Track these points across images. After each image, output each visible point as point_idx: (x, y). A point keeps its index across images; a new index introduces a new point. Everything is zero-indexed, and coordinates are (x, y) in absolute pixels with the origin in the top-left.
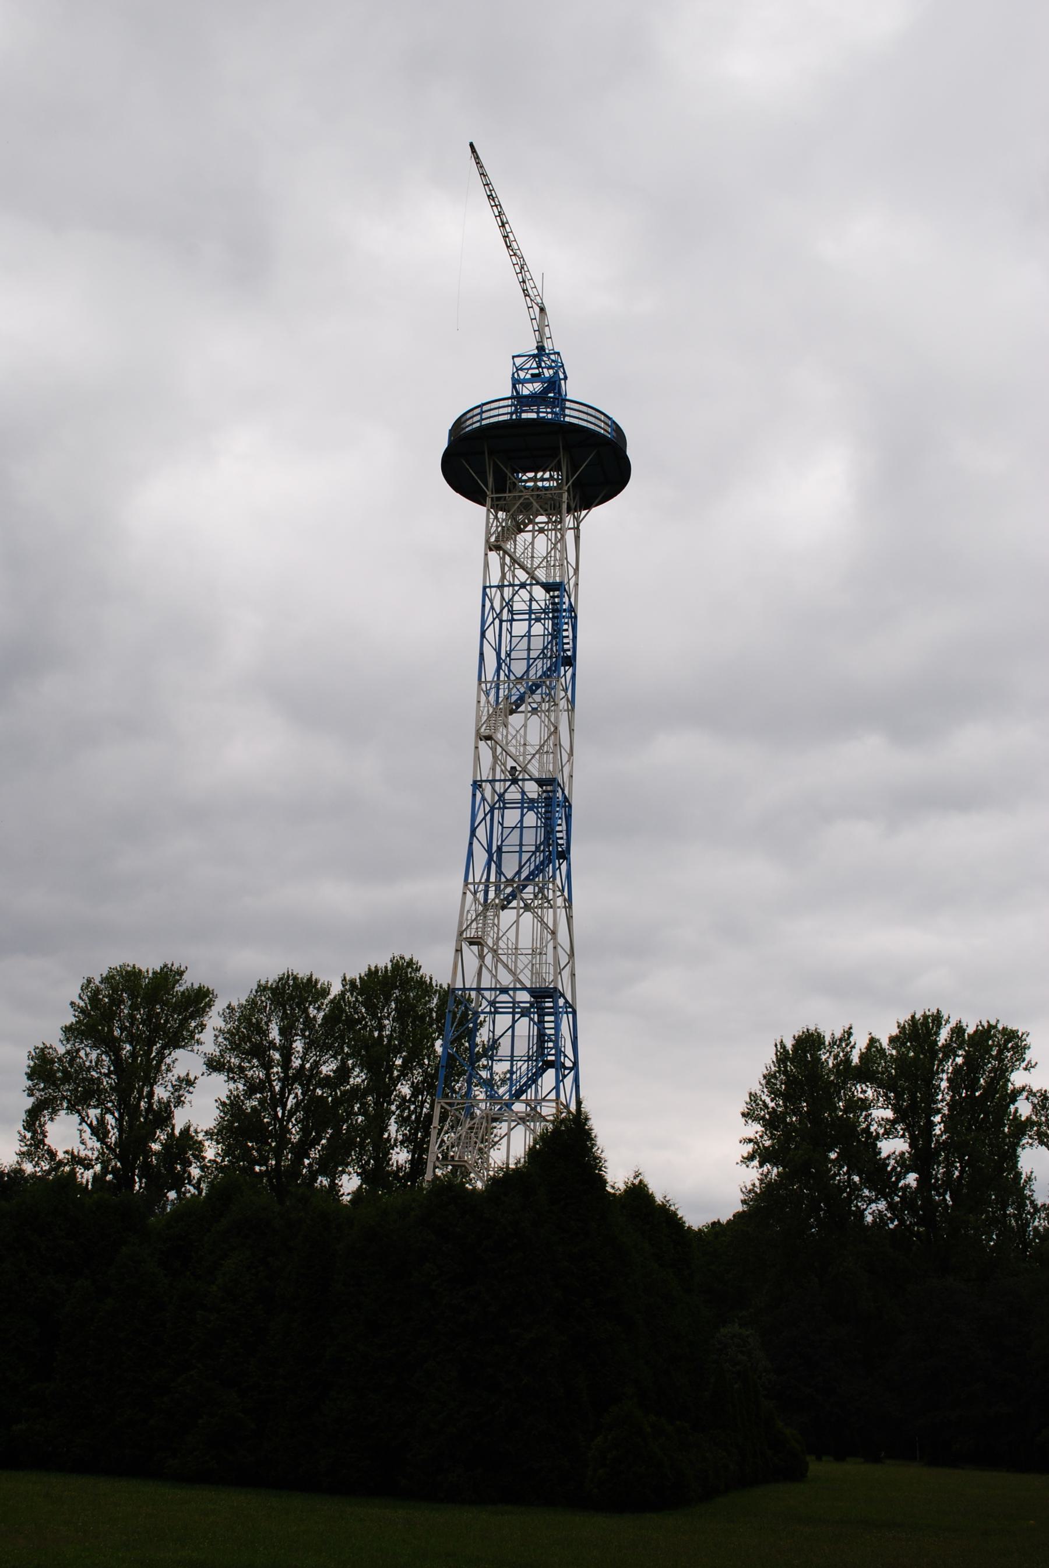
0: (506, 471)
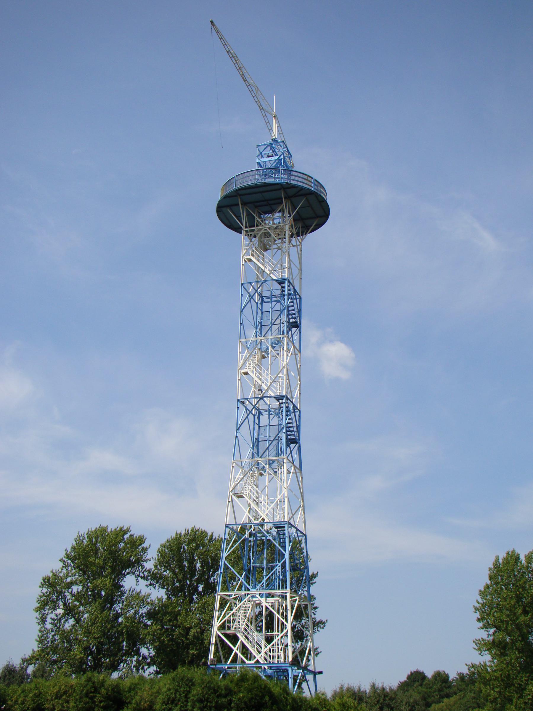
0: (255, 216)
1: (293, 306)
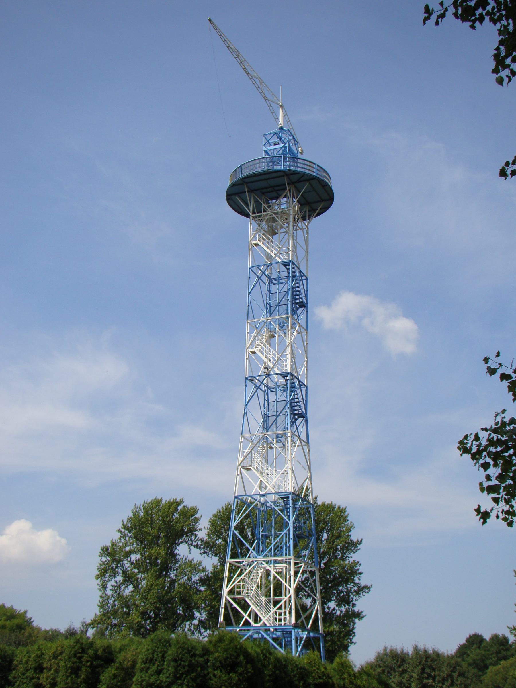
1: (298, 287)
